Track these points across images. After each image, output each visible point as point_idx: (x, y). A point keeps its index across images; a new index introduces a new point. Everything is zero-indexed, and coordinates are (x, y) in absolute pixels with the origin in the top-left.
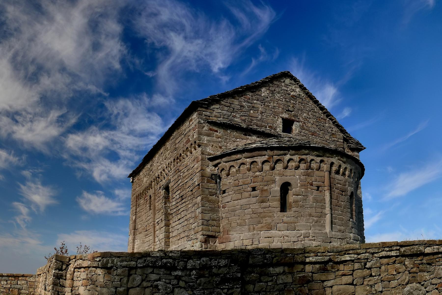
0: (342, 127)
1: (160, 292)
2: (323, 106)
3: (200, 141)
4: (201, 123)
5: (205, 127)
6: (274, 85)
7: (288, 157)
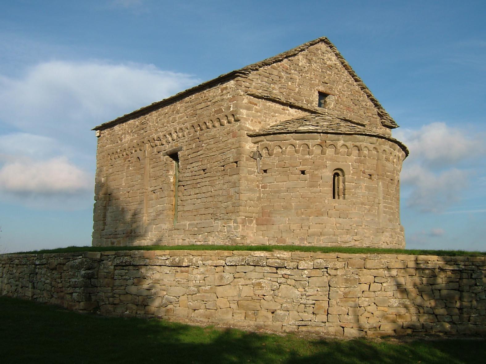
0: (377, 102)
1: (264, 289)
4: (241, 95)
5: (245, 100)
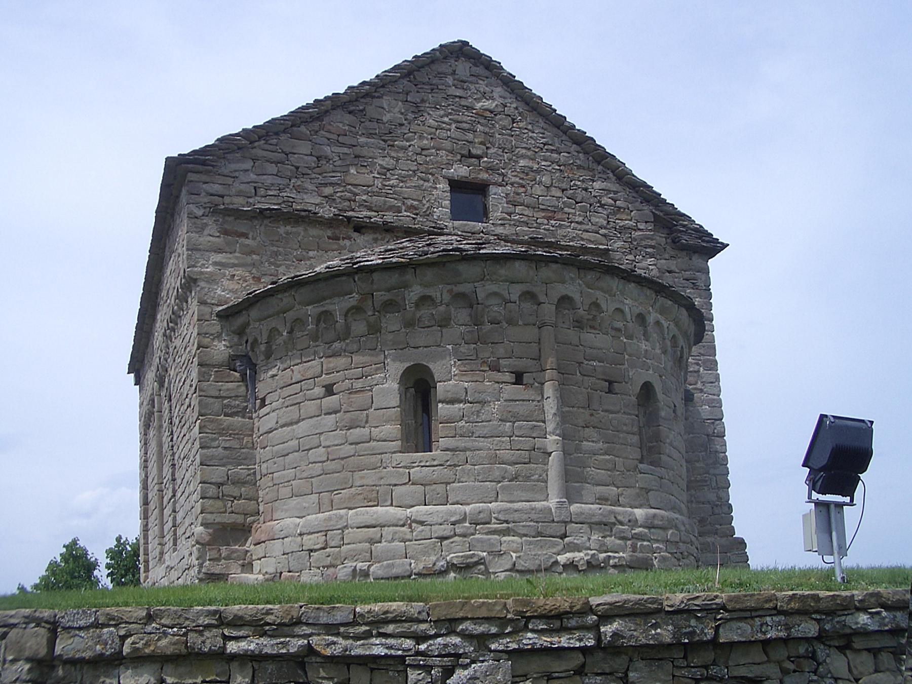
2: (579, 130)
3: (194, 266)
4: (196, 218)
6: (422, 86)
7: (415, 292)
